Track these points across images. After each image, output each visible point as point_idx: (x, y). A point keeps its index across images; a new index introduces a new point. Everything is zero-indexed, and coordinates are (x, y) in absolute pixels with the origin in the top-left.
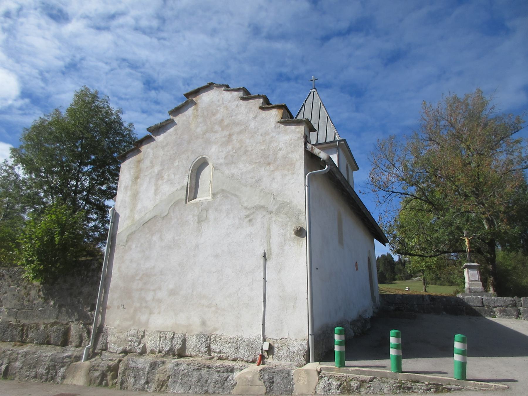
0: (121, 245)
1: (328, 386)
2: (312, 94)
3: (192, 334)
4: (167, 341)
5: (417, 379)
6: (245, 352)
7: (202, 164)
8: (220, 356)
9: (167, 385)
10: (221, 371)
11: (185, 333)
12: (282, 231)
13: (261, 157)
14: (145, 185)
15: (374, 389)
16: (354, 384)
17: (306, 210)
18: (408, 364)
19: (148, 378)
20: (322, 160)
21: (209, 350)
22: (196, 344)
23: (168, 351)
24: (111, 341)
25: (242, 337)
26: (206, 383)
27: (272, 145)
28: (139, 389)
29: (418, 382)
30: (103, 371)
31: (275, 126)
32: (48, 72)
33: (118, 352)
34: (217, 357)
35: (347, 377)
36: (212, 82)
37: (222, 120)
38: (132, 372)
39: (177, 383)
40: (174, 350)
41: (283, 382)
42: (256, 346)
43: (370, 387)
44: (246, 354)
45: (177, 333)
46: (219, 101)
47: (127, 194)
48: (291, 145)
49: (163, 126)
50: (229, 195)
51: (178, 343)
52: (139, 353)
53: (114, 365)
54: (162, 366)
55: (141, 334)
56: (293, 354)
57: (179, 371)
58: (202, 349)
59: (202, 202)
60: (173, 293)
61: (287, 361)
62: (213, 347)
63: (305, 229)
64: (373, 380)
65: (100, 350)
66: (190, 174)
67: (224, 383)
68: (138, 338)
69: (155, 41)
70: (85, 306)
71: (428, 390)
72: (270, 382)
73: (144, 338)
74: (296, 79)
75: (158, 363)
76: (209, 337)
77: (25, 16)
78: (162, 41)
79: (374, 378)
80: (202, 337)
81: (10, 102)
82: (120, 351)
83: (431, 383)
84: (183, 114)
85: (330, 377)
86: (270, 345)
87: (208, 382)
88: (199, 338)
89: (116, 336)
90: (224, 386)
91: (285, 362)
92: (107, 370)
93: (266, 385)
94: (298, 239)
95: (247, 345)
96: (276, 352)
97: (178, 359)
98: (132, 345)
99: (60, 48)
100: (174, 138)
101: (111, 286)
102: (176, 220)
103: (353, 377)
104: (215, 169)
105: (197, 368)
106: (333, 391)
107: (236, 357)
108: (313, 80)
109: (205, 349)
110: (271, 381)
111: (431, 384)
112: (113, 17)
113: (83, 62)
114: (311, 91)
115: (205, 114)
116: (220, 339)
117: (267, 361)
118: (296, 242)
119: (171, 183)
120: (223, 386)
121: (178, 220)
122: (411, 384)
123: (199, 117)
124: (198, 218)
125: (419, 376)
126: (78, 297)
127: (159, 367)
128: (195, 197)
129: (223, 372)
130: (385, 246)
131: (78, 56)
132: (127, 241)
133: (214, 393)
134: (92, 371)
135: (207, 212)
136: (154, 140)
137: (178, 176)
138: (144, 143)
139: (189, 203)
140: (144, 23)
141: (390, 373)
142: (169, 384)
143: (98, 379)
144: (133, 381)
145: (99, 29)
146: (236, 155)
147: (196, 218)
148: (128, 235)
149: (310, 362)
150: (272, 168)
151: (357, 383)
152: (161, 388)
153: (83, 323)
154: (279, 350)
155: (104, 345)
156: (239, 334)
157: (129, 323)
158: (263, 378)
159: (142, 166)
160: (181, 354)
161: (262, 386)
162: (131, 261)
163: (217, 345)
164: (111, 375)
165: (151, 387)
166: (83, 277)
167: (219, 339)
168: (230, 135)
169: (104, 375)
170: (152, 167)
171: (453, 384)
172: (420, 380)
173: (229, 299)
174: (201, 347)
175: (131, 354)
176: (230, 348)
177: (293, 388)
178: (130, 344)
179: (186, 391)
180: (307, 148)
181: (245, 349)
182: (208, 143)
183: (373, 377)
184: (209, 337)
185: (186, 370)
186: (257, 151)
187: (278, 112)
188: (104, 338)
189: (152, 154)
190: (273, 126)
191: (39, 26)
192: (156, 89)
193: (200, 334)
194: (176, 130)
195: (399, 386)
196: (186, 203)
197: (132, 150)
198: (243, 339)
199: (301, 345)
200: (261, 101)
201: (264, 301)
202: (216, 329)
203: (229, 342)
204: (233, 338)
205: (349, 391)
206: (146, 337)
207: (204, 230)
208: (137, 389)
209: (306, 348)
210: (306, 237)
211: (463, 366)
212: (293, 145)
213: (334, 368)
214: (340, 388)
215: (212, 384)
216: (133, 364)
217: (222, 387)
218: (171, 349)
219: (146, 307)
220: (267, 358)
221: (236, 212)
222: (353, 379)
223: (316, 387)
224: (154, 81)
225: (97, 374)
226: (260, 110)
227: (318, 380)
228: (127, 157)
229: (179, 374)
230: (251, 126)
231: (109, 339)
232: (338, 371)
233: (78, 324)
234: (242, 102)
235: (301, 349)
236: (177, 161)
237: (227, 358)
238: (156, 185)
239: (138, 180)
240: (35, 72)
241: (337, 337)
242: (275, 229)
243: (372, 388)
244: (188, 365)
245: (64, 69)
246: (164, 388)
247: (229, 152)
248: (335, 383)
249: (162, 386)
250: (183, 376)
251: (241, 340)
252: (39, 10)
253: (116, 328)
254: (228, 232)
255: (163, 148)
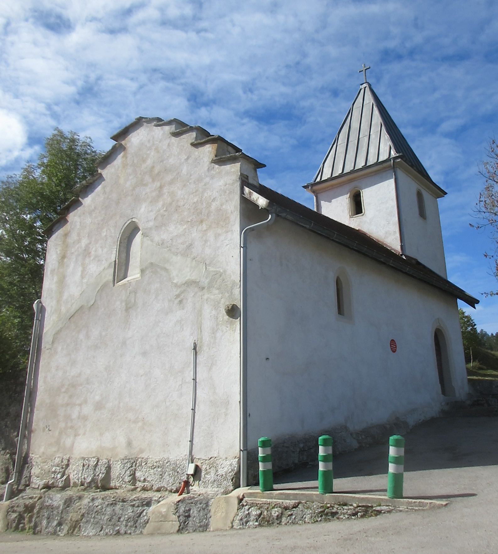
0: (47, 348)
1: (246, 517)
2: (362, 91)
3: (117, 459)
4: (89, 471)
5: (345, 501)
6: (170, 478)
7: (133, 230)
8: (144, 486)
9: (80, 526)
10: (136, 505)
11: (110, 458)
12: (214, 312)
13: (193, 213)
14: (72, 265)
15: (295, 518)
16: (274, 512)
17: (240, 281)
18: (339, 483)
19: (61, 518)
20: (260, 208)
21: (134, 479)
22: (120, 471)
23: (90, 483)
24: (35, 473)
25: (168, 458)
26: (119, 521)
27: (206, 195)
28: (51, 532)
29: (345, 505)
30: (20, 512)
31: (209, 168)
32: (57, 104)
33: (40, 488)
34: (141, 488)
35: (269, 504)
36: (140, 117)
37: (153, 167)
38: (46, 512)
39: (89, 523)
40: (98, 481)
41: (199, 515)
42: (182, 470)
43: (292, 515)
44: (170, 481)
45: (101, 458)
46: (149, 141)
47: (53, 280)
48: (226, 192)
49: (91, 183)
50: (159, 270)
51: (102, 472)
52: (60, 487)
53: (31, 504)
54: (79, 502)
55: (65, 462)
56: (221, 477)
57: (94, 508)
58: (126, 478)
59: (130, 282)
60: (99, 406)
61: (213, 488)
62: (138, 474)
63: (239, 307)
64: (298, 505)
65: (23, 485)
66: (118, 246)
67: (137, 521)
68: (63, 468)
69: (193, 35)
70: (12, 431)
71: (354, 514)
72: (186, 516)
73: (69, 468)
74: (412, 53)
75: (74, 499)
76: (134, 462)
77: (16, 32)
78: (202, 34)
79: (299, 503)
80: (127, 462)
81: (16, 154)
82: (42, 486)
83: (360, 505)
84: (112, 164)
85: (252, 505)
86: (197, 467)
87: (122, 519)
88: (124, 464)
89: (40, 467)
90: (137, 524)
91: (211, 489)
92: (24, 510)
93: (181, 520)
94: (231, 322)
95: (173, 470)
96: (204, 476)
97: (100, 491)
98: (55, 477)
99: (67, 69)
100: (102, 198)
101: (37, 403)
102: (103, 309)
103: (275, 503)
104: (144, 236)
105: (111, 502)
106: (251, 523)
107: (159, 486)
108: (364, 71)
109: (128, 478)
110: (187, 514)
111: (359, 506)
112: (129, 12)
113: (99, 82)
114: (361, 87)
115: (135, 161)
116: (146, 464)
117: (192, 489)
118: (229, 326)
119: (99, 261)
120: (135, 524)
121: (105, 309)
122: (337, 508)
123: (129, 167)
124: (126, 304)
125: (348, 496)
126: (6, 420)
127: (75, 503)
128: (125, 277)
129: (138, 506)
130: (475, 308)
131: (93, 76)
132: (53, 342)
133: (126, 533)
134: (10, 513)
135: (135, 295)
136: (81, 204)
137: (105, 250)
138: (71, 209)
139: (117, 285)
140: (173, 12)
141: (316, 495)
142: (82, 524)
143: (14, 523)
144: (46, 523)
145: (112, 32)
146: (166, 213)
147: (124, 304)
148: (54, 335)
149: (239, 487)
150: (204, 227)
151: (278, 512)
152: (74, 530)
153: (10, 452)
154: (207, 474)
155: (27, 479)
156: (166, 456)
157: (54, 449)
158: (178, 511)
159: (70, 240)
160: (105, 486)
161: (175, 521)
162: (57, 368)
163: (142, 472)
164: (28, 516)
165: (63, 529)
166: (11, 393)
167: (145, 463)
168: (161, 187)
169: (21, 518)
170: (79, 241)
171: (384, 504)
172: (348, 502)
173: (156, 410)
174: (125, 475)
175: (54, 488)
176: (155, 474)
177: (209, 522)
178: (53, 476)
179: (97, 533)
180: (244, 194)
181: (170, 474)
182: (137, 200)
183: (299, 501)
184: (134, 462)
185: (100, 505)
186: (189, 205)
187: (212, 148)
188: (27, 471)
189: (79, 223)
190: (206, 168)
191: (35, 43)
192: (206, 105)
193: (126, 458)
194: (104, 188)
195: (321, 512)
196: (114, 286)
197: (58, 221)
198: (169, 461)
199: (231, 465)
200: (194, 134)
201: (193, 410)
202: (142, 451)
203: (155, 466)
204: (159, 461)
205: (268, 521)
206: (70, 466)
207: (132, 319)
208: (48, 533)
209: (236, 468)
210: (239, 318)
211: (398, 480)
212: (228, 192)
213: (257, 493)
214: (259, 519)
215: (124, 523)
216: (49, 502)
217: (135, 525)
218: (93, 480)
219: (72, 427)
220: (192, 484)
221: (166, 292)
222: (276, 506)
223: (233, 520)
224: (202, 94)
225: (14, 515)
226: (193, 148)
227: (238, 510)
228: (53, 230)
229: (93, 511)
230: (183, 172)
231: (33, 471)
232: (262, 496)
233: (5, 454)
234: (174, 139)
235: (230, 470)
236: (105, 230)
237: (151, 489)
238: (83, 265)
239: (65, 260)
240: (41, 107)
241: (321, 451)
242: (208, 311)
243: (294, 517)
244: (103, 499)
245: (77, 97)
246: (77, 529)
247: (159, 211)
248: (255, 512)
249: (75, 527)
250: (96, 514)
251: (167, 463)
252: (31, 20)
253: (40, 457)
254: (157, 320)
255: (90, 213)
